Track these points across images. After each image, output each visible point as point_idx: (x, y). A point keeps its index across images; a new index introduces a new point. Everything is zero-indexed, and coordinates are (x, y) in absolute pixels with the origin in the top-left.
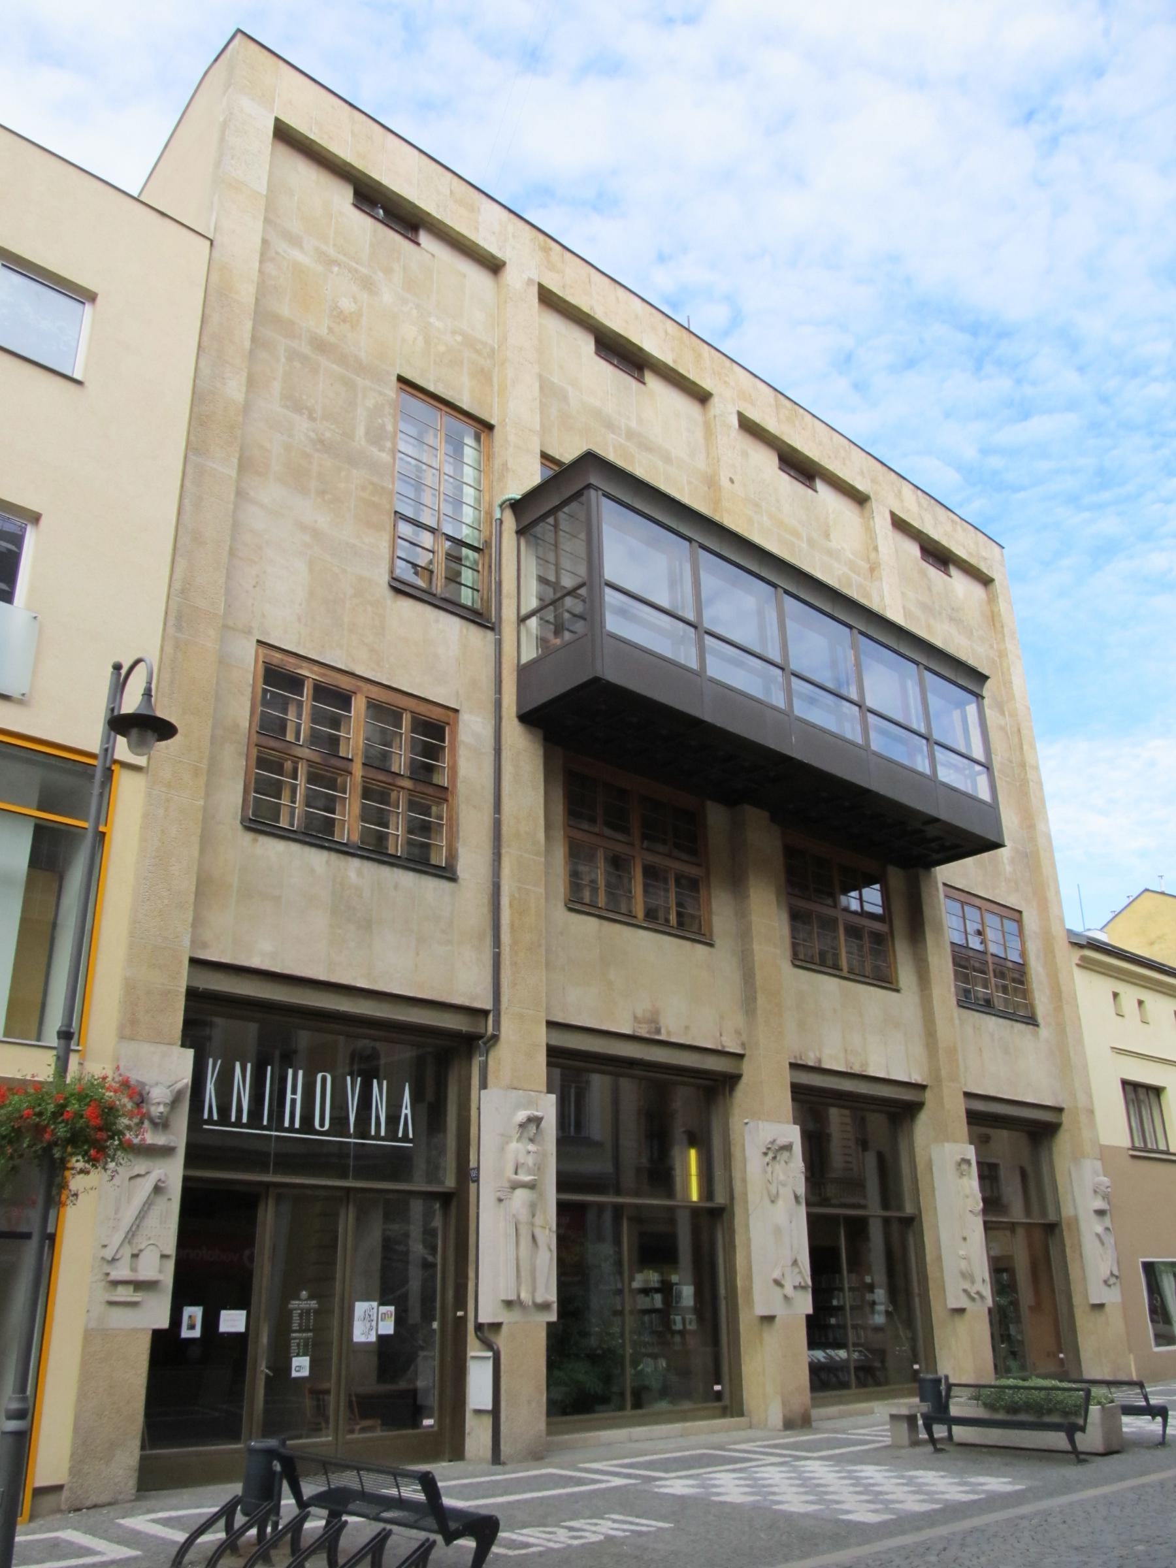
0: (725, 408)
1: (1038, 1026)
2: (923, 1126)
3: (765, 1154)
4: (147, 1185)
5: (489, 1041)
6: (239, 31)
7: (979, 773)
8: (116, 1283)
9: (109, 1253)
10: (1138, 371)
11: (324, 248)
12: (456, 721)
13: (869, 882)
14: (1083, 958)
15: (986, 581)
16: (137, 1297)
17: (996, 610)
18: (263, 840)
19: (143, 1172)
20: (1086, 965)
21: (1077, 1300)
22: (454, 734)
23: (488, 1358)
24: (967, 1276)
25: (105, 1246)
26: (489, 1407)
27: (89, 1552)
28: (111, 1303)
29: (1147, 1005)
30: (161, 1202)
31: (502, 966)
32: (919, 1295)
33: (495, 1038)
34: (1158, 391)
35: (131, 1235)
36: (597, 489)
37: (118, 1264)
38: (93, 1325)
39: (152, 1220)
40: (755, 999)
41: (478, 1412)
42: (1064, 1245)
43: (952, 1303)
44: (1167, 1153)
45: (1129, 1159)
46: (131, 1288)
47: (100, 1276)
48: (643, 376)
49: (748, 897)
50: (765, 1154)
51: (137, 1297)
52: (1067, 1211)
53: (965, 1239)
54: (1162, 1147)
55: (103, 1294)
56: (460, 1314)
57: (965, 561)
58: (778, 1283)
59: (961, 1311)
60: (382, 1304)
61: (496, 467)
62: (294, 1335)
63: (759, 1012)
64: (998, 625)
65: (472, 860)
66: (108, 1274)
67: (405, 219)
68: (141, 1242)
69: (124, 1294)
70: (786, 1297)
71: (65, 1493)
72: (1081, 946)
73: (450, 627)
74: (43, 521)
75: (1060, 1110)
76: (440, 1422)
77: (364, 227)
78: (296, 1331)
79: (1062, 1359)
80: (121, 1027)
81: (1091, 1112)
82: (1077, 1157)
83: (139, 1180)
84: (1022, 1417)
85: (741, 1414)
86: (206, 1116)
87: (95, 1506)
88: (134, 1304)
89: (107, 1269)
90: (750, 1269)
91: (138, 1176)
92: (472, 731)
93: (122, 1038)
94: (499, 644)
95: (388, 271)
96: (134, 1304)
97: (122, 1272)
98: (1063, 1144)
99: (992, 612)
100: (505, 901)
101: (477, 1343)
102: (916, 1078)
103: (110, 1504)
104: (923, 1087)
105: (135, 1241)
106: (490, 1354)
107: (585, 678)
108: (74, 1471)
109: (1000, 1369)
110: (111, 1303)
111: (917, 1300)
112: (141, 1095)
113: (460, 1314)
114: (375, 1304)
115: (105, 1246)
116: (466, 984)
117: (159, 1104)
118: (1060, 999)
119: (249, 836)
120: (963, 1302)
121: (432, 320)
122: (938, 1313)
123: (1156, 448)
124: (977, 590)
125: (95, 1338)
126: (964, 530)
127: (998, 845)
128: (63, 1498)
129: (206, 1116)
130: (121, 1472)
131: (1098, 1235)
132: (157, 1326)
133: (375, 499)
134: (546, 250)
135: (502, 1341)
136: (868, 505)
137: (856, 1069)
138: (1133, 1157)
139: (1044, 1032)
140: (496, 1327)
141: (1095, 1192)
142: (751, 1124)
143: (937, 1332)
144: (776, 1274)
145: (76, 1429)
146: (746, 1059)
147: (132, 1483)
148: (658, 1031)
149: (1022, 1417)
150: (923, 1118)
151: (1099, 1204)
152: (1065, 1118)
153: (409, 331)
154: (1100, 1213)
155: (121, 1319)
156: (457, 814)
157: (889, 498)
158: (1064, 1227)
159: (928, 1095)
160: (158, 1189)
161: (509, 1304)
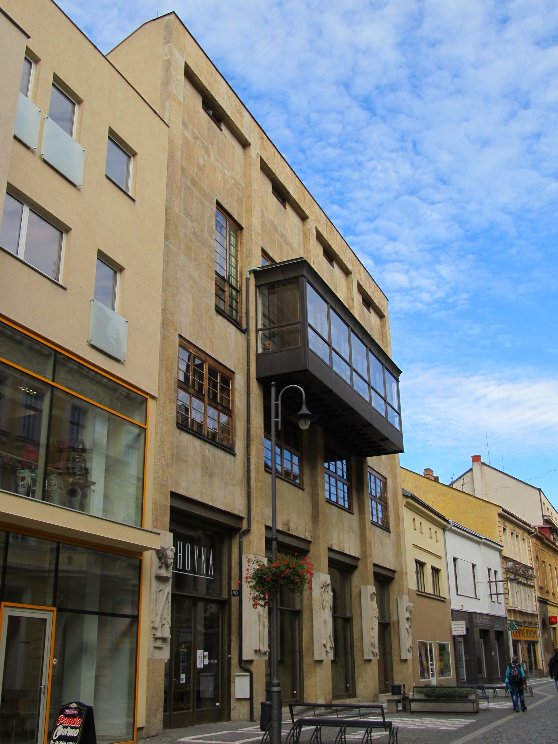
0: (312, 224)
1: (390, 532)
2: (356, 577)
3: (322, 588)
5: (243, 533)
6: (174, 12)
7: (396, 416)
8: (156, 639)
10: (322, 137)
11: (194, 129)
12: (234, 376)
13: (341, 459)
14: (407, 502)
15: (381, 316)
17: (384, 331)
18: (182, 433)
20: (408, 505)
21: (395, 658)
22: (233, 383)
23: (247, 675)
24: (373, 645)
26: (248, 697)
27: (538, 690)
28: (155, 648)
29: (423, 524)
31: (252, 496)
32: (351, 654)
33: (248, 531)
34: (331, 153)
36: (305, 277)
38: (150, 657)
40: (318, 516)
41: (239, 699)
42: (391, 633)
43: (366, 657)
44: (424, 593)
45: (416, 596)
47: (152, 636)
48: (285, 204)
49: (317, 468)
50: (322, 588)
52: (394, 618)
53: (372, 629)
54: (423, 591)
55: (153, 644)
56: (229, 656)
57: (377, 306)
58: (325, 646)
59: (370, 661)
60: (204, 651)
61: (244, 250)
62: (181, 664)
63: (320, 522)
64: (385, 339)
65: (240, 448)
67: (218, 116)
70: (327, 651)
71: (144, 731)
72: (407, 497)
73: (232, 329)
74: (125, 271)
75: (394, 572)
76: (222, 704)
77: (204, 117)
78: (181, 663)
79: (387, 684)
80: (153, 523)
81: (406, 573)
82: (401, 594)
85: (355, 697)
87: (153, 736)
90: (312, 639)
92: (239, 382)
94: (248, 341)
95: (213, 144)
97: (159, 635)
98: (394, 587)
99: (383, 332)
100: (253, 467)
101: (238, 668)
102: (357, 555)
103: (157, 735)
104: (357, 559)
106: (248, 674)
107: (299, 368)
108: (147, 722)
109: (267, 699)
110: (155, 648)
111: (350, 656)
112: (163, 554)
113: (229, 656)
114: (203, 651)
116: (237, 506)
118: (399, 521)
119: (177, 431)
120: (371, 657)
121: (226, 171)
122: (358, 661)
123: (326, 185)
124: (378, 319)
125: (151, 661)
126: (377, 290)
127: (402, 451)
128: (143, 733)
130: (159, 722)
131: (407, 629)
133: (210, 264)
134: (262, 138)
135: (253, 668)
136: (350, 276)
137: (341, 550)
138: (417, 594)
139: (392, 535)
140: (251, 662)
141: (407, 609)
142: (316, 574)
143: (357, 670)
144: (324, 642)
145: (147, 703)
146: (312, 544)
147: (162, 726)
148: (289, 530)
150: (357, 573)
151: (408, 615)
152: (396, 576)
153: (219, 177)
154: (408, 619)
156: (235, 424)
157: (358, 275)
158: (391, 624)
159: (360, 563)
161: (256, 651)
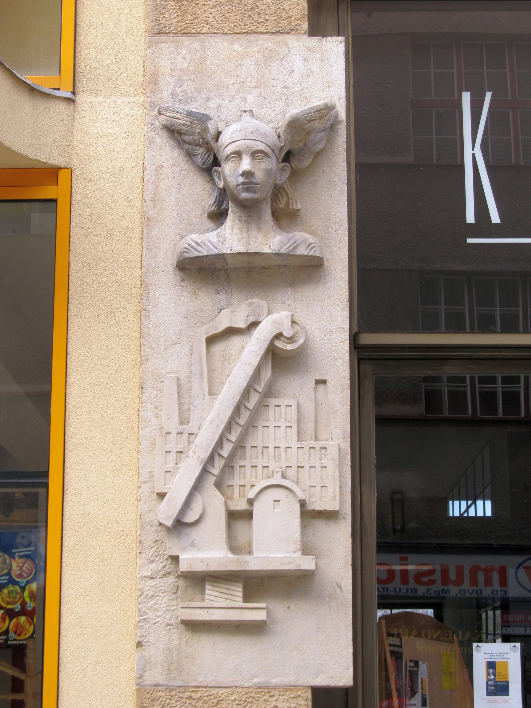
4: (249, 352)
8: (199, 580)
9: (167, 512)
16: (256, 613)
19: (242, 325)
25: (162, 496)
30: (295, 394)
35: (222, 464)
37: (195, 534)
38: (156, 676)
39: (277, 430)
46: (238, 591)
51: (256, 613)
55: (169, 606)
66: (175, 559)
68: (249, 479)
69: (222, 604)
83: (235, 341)
84: (254, 398)
86: (471, 218)
88: (255, 629)
89: (173, 547)
91: (231, 332)
93: (158, 32)
96: (255, 629)
97: (208, 551)
105: (236, 481)
110: (193, 626)
115: (162, 496)
117: (238, 154)
129: (471, 218)
132: (321, 681)
149: (254, 398)
155: (220, 663)
160: (281, 359)
